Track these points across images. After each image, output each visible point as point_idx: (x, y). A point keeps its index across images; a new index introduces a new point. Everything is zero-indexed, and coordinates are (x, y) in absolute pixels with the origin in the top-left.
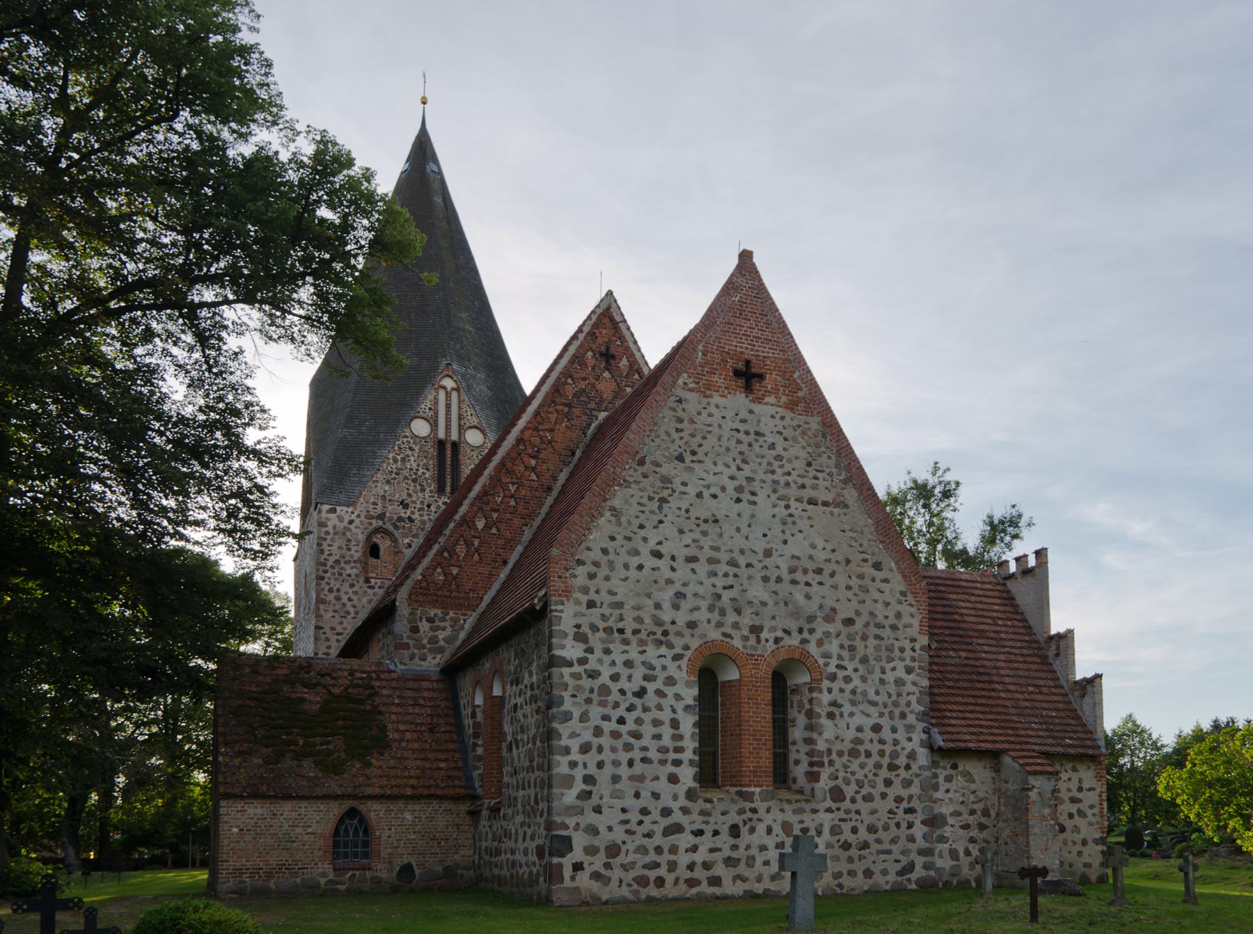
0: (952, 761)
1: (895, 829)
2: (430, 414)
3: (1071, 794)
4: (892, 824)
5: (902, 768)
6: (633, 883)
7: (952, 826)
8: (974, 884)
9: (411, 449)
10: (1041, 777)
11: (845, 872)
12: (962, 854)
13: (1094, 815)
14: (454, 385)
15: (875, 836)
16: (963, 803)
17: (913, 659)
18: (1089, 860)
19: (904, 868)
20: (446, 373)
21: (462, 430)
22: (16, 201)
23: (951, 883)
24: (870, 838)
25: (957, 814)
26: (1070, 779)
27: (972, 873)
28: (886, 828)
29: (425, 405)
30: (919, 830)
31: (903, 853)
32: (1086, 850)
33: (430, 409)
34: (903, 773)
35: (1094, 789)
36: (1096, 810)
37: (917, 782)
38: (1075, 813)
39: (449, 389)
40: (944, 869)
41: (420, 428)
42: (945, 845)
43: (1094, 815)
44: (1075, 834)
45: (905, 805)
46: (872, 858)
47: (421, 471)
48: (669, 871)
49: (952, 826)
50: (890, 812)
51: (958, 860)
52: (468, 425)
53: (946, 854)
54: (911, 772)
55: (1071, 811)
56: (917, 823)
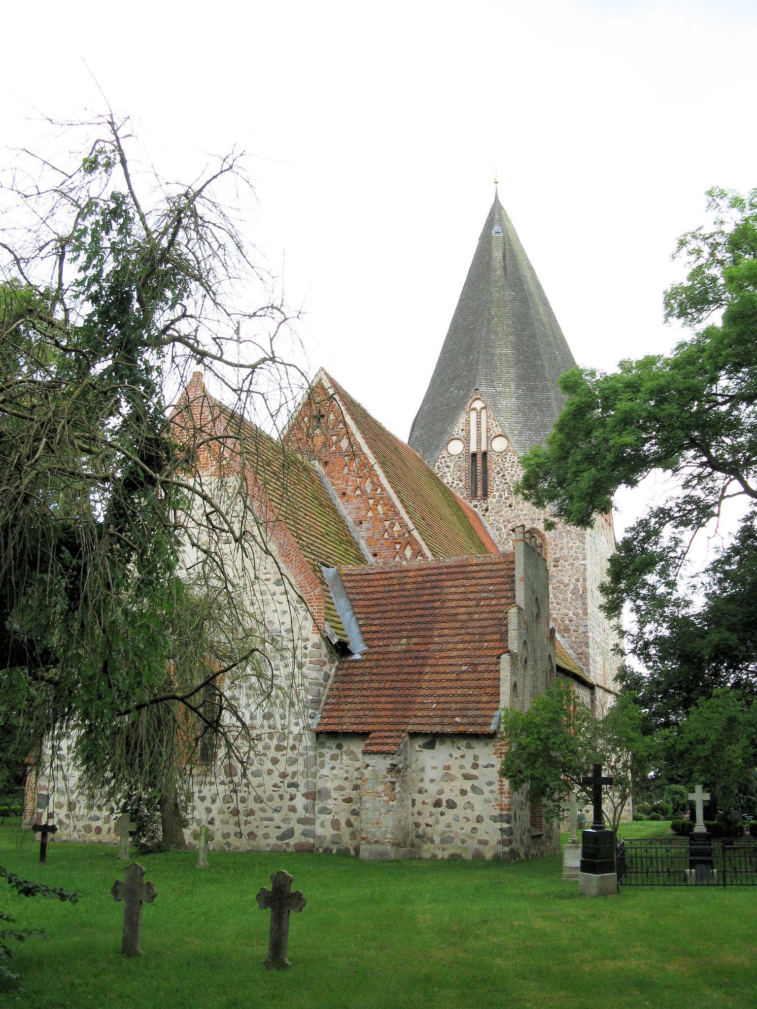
0: (337, 742)
1: (279, 800)
2: (463, 434)
3: (464, 771)
4: (276, 796)
5: (289, 749)
6: (82, 829)
7: (335, 799)
8: (352, 853)
9: (448, 467)
10: (377, 757)
11: (232, 834)
12: (343, 825)
13: (492, 792)
14: (483, 405)
15: (261, 805)
16: (346, 779)
17: (305, 655)
18: (485, 837)
19: (284, 834)
20: (475, 397)
21: (490, 440)
22: (142, 388)
23: (331, 851)
24: (256, 806)
25: (341, 788)
26: (463, 757)
27: (352, 842)
28: (271, 799)
29: (458, 429)
30: (300, 802)
31: (284, 821)
32: (481, 827)
33: (462, 430)
34: (290, 753)
35: (492, 766)
36: (495, 788)
37: (301, 760)
38: (469, 789)
39: (479, 409)
40: (325, 837)
41: (456, 447)
42: (328, 816)
43: (492, 792)
44: (469, 811)
45: (287, 780)
46: (256, 824)
47: (456, 482)
48: (105, 823)
49: (335, 799)
50: (275, 786)
51: (338, 829)
52: (494, 435)
53: (328, 824)
54: (296, 752)
55: (464, 788)
56: (299, 795)
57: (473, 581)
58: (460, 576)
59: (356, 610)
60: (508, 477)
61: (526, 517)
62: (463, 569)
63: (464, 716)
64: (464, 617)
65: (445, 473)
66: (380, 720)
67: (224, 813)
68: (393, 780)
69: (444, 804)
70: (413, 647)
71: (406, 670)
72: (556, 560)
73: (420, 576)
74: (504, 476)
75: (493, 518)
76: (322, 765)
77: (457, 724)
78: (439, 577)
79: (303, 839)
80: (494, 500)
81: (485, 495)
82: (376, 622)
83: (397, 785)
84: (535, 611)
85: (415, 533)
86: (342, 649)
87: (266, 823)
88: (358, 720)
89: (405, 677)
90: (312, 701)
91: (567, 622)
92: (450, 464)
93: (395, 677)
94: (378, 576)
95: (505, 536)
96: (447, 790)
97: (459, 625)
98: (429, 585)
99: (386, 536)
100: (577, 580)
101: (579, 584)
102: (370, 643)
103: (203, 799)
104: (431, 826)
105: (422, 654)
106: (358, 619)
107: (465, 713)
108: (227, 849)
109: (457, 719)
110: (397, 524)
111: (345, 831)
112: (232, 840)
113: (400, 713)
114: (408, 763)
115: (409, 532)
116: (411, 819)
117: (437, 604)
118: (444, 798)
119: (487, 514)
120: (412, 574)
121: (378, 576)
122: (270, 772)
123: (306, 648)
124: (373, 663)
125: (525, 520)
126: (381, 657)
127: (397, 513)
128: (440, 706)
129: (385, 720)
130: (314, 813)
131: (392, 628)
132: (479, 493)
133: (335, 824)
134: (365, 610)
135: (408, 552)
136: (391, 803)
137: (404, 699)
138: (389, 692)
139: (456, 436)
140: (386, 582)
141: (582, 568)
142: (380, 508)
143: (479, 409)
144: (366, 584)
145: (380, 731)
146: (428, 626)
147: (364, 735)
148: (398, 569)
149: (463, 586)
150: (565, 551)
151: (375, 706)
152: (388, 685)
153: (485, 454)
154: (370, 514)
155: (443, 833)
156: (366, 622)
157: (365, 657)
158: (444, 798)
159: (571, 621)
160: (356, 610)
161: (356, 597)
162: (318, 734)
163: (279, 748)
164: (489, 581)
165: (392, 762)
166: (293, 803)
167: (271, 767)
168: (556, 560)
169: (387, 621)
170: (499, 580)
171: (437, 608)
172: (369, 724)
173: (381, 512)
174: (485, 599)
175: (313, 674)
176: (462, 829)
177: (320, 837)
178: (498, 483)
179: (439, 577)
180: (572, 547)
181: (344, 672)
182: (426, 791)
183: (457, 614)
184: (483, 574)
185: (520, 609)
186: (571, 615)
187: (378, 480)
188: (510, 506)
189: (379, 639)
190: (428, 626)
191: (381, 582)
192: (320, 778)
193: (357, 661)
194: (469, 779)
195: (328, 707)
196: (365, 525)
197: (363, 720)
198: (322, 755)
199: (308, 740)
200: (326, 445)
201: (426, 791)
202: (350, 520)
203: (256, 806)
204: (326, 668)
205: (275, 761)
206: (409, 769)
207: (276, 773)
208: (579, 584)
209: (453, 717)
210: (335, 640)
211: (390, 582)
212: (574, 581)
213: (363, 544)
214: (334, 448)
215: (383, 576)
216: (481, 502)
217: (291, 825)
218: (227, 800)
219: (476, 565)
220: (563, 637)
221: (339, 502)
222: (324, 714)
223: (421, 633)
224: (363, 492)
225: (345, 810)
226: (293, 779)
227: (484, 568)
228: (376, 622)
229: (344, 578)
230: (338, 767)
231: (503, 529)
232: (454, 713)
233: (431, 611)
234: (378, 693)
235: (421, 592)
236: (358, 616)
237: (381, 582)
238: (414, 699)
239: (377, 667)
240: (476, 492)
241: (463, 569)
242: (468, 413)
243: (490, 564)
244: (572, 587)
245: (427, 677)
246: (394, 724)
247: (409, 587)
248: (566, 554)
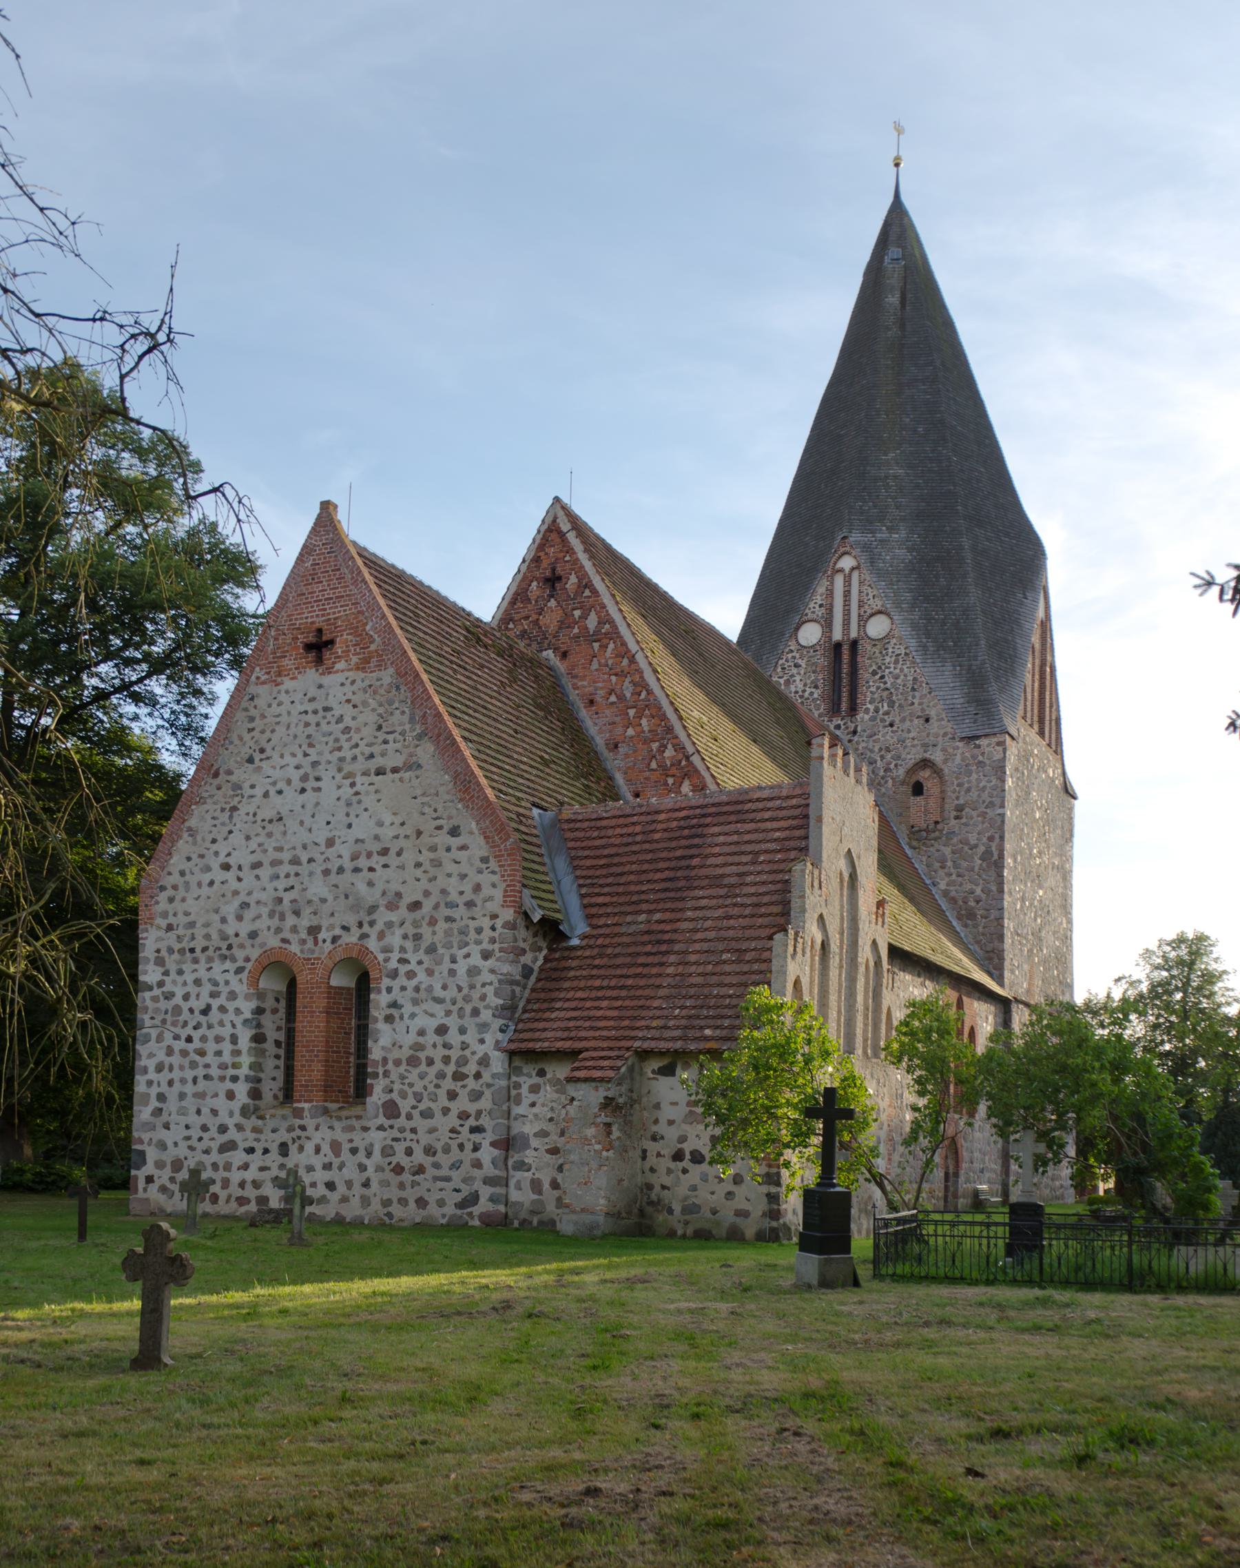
0: (538, 1067)
4: (454, 1145)
7: (536, 1150)
9: (797, 666)
11: (395, 1200)
12: (546, 1186)
16: (551, 1120)
18: (745, 1206)
20: (842, 550)
23: (531, 1223)
24: (427, 1161)
25: (543, 1134)
28: (447, 1150)
29: (814, 605)
30: (487, 1154)
31: (464, 1181)
32: (740, 1191)
33: (821, 606)
34: (471, 1083)
37: (488, 1094)
41: (810, 634)
42: (526, 1174)
46: (427, 1185)
48: (223, 1188)
49: (536, 1150)
50: (453, 1131)
51: (540, 1193)
52: (869, 612)
53: (526, 1185)
54: (481, 1081)
56: (486, 1144)
57: (752, 826)
58: (733, 818)
59: (578, 873)
60: (889, 680)
61: (916, 742)
62: (739, 807)
63: (717, 1027)
64: (733, 880)
65: (793, 676)
66: (597, 1034)
67: (383, 1170)
68: (608, 1120)
69: (688, 1156)
70: (656, 927)
71: (641, 960)
72: (960, 809)
73: (675, 819)
74: (882, 677)
75: (864, 744)
76: (518, 1101)
77: (707, 1039)
78: (702, 821)
79: (491, 1207)
80: (867, 717)
81: (853, 709)
82: (606, 890)
83: (614, 1128)
86: (551, 930)
87: (440, 1184)
88: (566, 1034)
89: (639, 970)
90: (503, 1007)
91: (972, 904)
92: (800, 661)
93: (624, 971)
94: (613, 822)
95: (882, 773)
97: (722, 892)
98: (686, 832)
99: (654, 765)
100: (991, 839)
102: (595, 921)
103: (354, 1151)
104: (668, 1189)
105: (666, 937)
106: (580, 886)
107: (719, 1022)
108: (388, 1222)
109: (708, 1032)
110: (670, 746)
111: (549, 1195)
112: (396, 1210)
113: (626, 1023)
114: (635, 1096)
115: (687, 758)
116: (640, 1180)
117: (695, 862)
118: (687, 1147)
119: (856, 738)
120: (662, 817)
121: (613, 822)
122: (446, 1111)
123: (493, 928)
124: (596, 951)
125: (913, 746)
126: (607, 941)
127: (670, 730)
128: (684, 1012)
129: (605, 1033)
130: (507, 1169)
131: (627, 899)
133: (536, 1186)
134: (590, 873)
136: (604, 1153)
137: (635, 1003)
138: (615, 993)
139: (810, 616)
140: (625, 831)
141: (999, 819)
142: (644, 722)
143: (847, 571)
144: (596, 834)
145: (595, 1049)
146: (679, 894)
147: (574, 1054)
148: (644, 809)
149: (737, 833)
150: (974, 794)
151: (592, 1013)
152: (613, 983)
153: (854, 644)
154: (630, 732)
155: (686, 1198)
156: (591, 890)
157: (584, 943)
158: (687, 1147)
159: (978, 902)
160: (578, 873)
161: (581, 853)
162: (512, 1054)
163: (459, 1076)
164: (775, 825)
165: (606, 1094)
166: (478, 1154)
167: (447, 1103)
168: (960, 809)
169: (621, 889)
170: (790, 822)
171: (694, 867)
172: (580, 1039)
173: (646, 729)
174: (766, 852)
175: (506, 968)
176: (713, 1193)
177: (515, 1204)
178: (873, 689)
179: (702, 821)
180: (985, 787)
181: (554, 964)
182: (662, 1138)
183: (723, 876)
184: (767, 815)
186: (978, 891)
187: (642, 677)
188: (891, 725)
189: (608, 915)
190: (679, 894)
191: (618, 831)
192: (516, 1119)
193: (574, 948)
195: (527, 1015)
196: (622, 749)
197: (573, 1034)
198: (518, 1086)
199: (498, 1063)
200: (566, 623)
201: (662, 1138)
202: (600, 741)
204: (527, 959)
205: (452, 1095)
206: (637, 1106)
209: (702, 1028)
210: (536, 918)
211: (630, 830)
212: (985, 840)
213: (619, 779)
214: (576, 630)
215: (621, 821)
216: (847, 719)
217: (475, 1187)
218: (387, 1151)
219: (758, 800)
220: (966, 926)
221: (583, 713)
222: (520, 1026)
223: (668, 905)
224: (621, 698)
225: (549, 1165)
226: (477, 1120)
227: (770, 804)
228: (606, 890)
229: (566, 826)
230: (540, 1101)
231: (879, 763)
232: (702, 1023)
233: (686, 873)
234: (600, 994)
235: (674, 844)
236: (581, 882)
237: (618, 831)
238: (648, 1003)
239: (601, 956)
240: (839, 705)
241: (739, 807)
242: (832, 576)
243: (779, 798)
244: (982, 849)
245: (670, 970)
246: (616, 1039)
247: (657, 836)
248: (975, 798)
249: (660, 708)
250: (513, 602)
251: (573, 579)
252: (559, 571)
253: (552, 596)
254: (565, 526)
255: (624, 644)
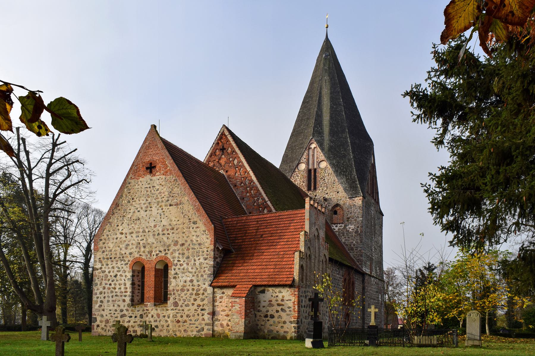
1: (197, 316)
3: (277, 302)
16: (226, 306)
24: (187, 319)
28: (194, 316)
35: (290, 300)
38: (280, 310)
41: (303, 166)
50: (195, 310)
52: (320, 160)
54: (204, 296)
56: (206, 314)
60: (326, 181)
69: (269, 316)
72: (348, 218)
81: (315, 188)
84: (316, 234)
85: (269, 203)
96: (270, 311)
101: (359, 229)
127: (260, 194)
132: (312, 188)
135: (266, 211)
143: (313, 148)
153: (315, 170)
154: (248, 194)
158: (269, 314)
166: (203, 317)
168: (348, 218)
185: (305, 232)
186: (354, 242)
194: (280, 306)
203: (187, 319)
207: (196, 305)
208: (359, 229)
217: (203, 326)
224: (245, 184)
249: (257, 188)
250: (211, 156)
251: (230, 149)
252: (225, 147)
253: (223, 154)
254: (227, 133)
255: (246, 169)
